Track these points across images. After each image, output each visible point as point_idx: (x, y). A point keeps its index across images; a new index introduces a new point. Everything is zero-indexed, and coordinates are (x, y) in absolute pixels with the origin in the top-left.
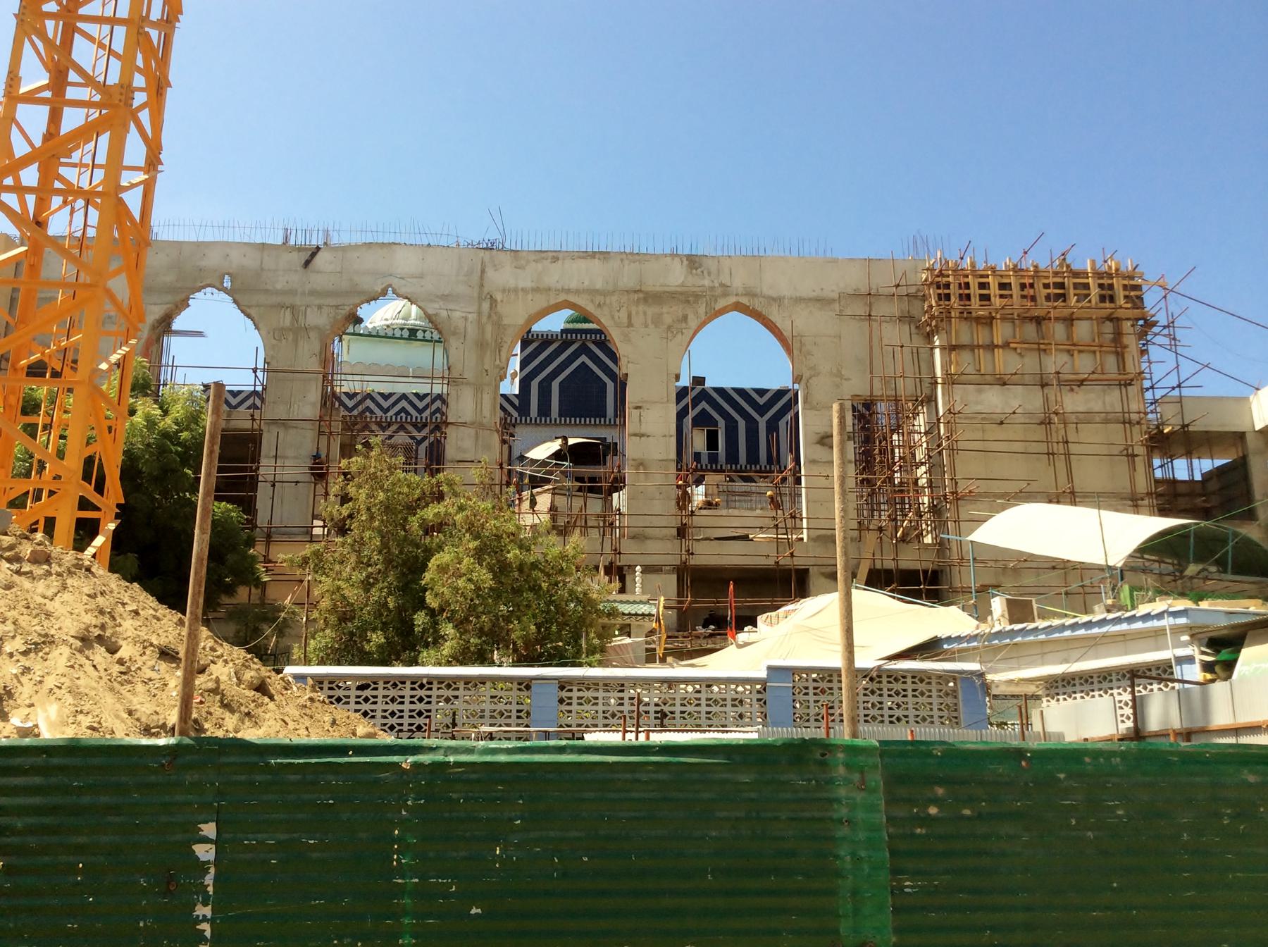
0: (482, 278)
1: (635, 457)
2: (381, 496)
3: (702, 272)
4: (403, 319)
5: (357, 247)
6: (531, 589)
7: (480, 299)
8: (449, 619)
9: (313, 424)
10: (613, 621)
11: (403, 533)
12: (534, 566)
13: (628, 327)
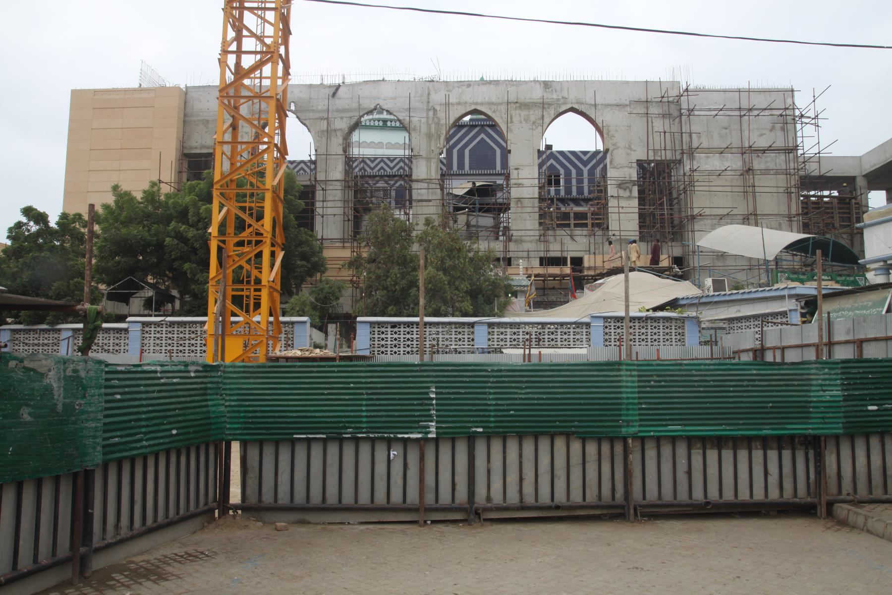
1: (516, 197)
3: (552, 90)
7: (428, 110)
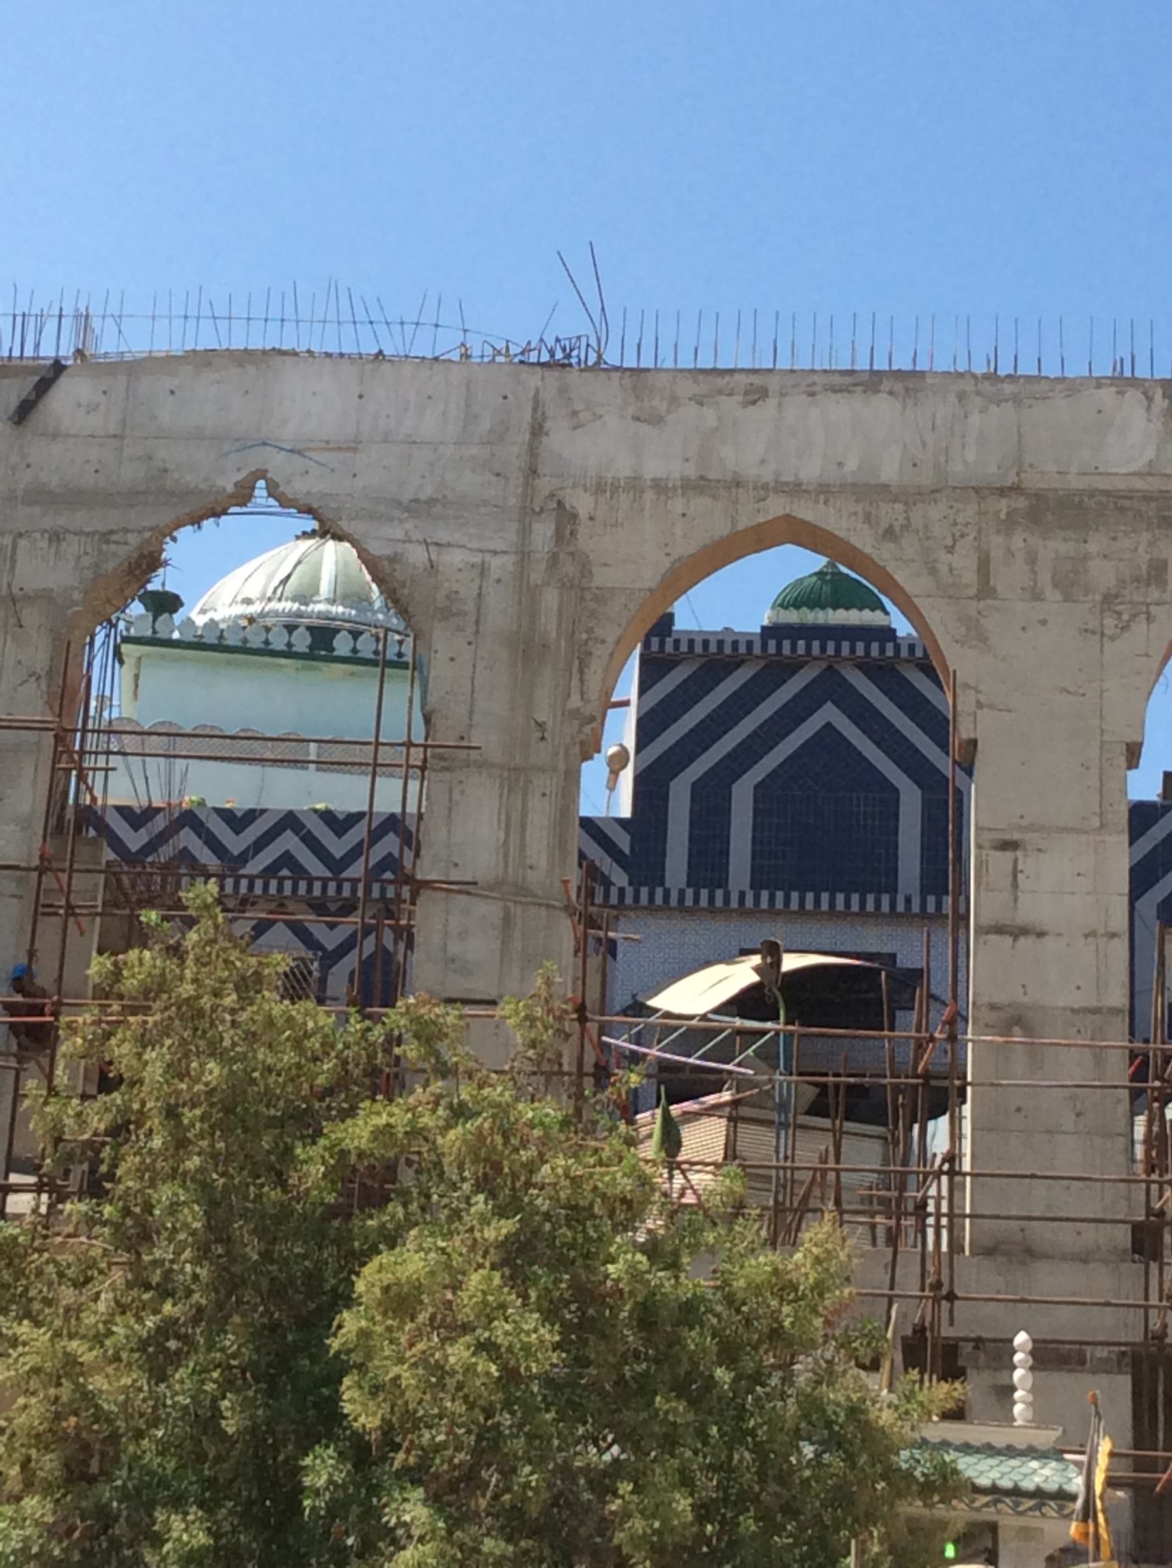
0: (533, 450)
2: (214, 1071)
4: (294, 600)
5: (169, 363)
6: (680, 1389)
7: (527, 514)
8: (414, 1475)
9: (20, 880)
10: (940, 1511)
11: (276, 1194)
12: (690, 1311)
13: (978, 597)
